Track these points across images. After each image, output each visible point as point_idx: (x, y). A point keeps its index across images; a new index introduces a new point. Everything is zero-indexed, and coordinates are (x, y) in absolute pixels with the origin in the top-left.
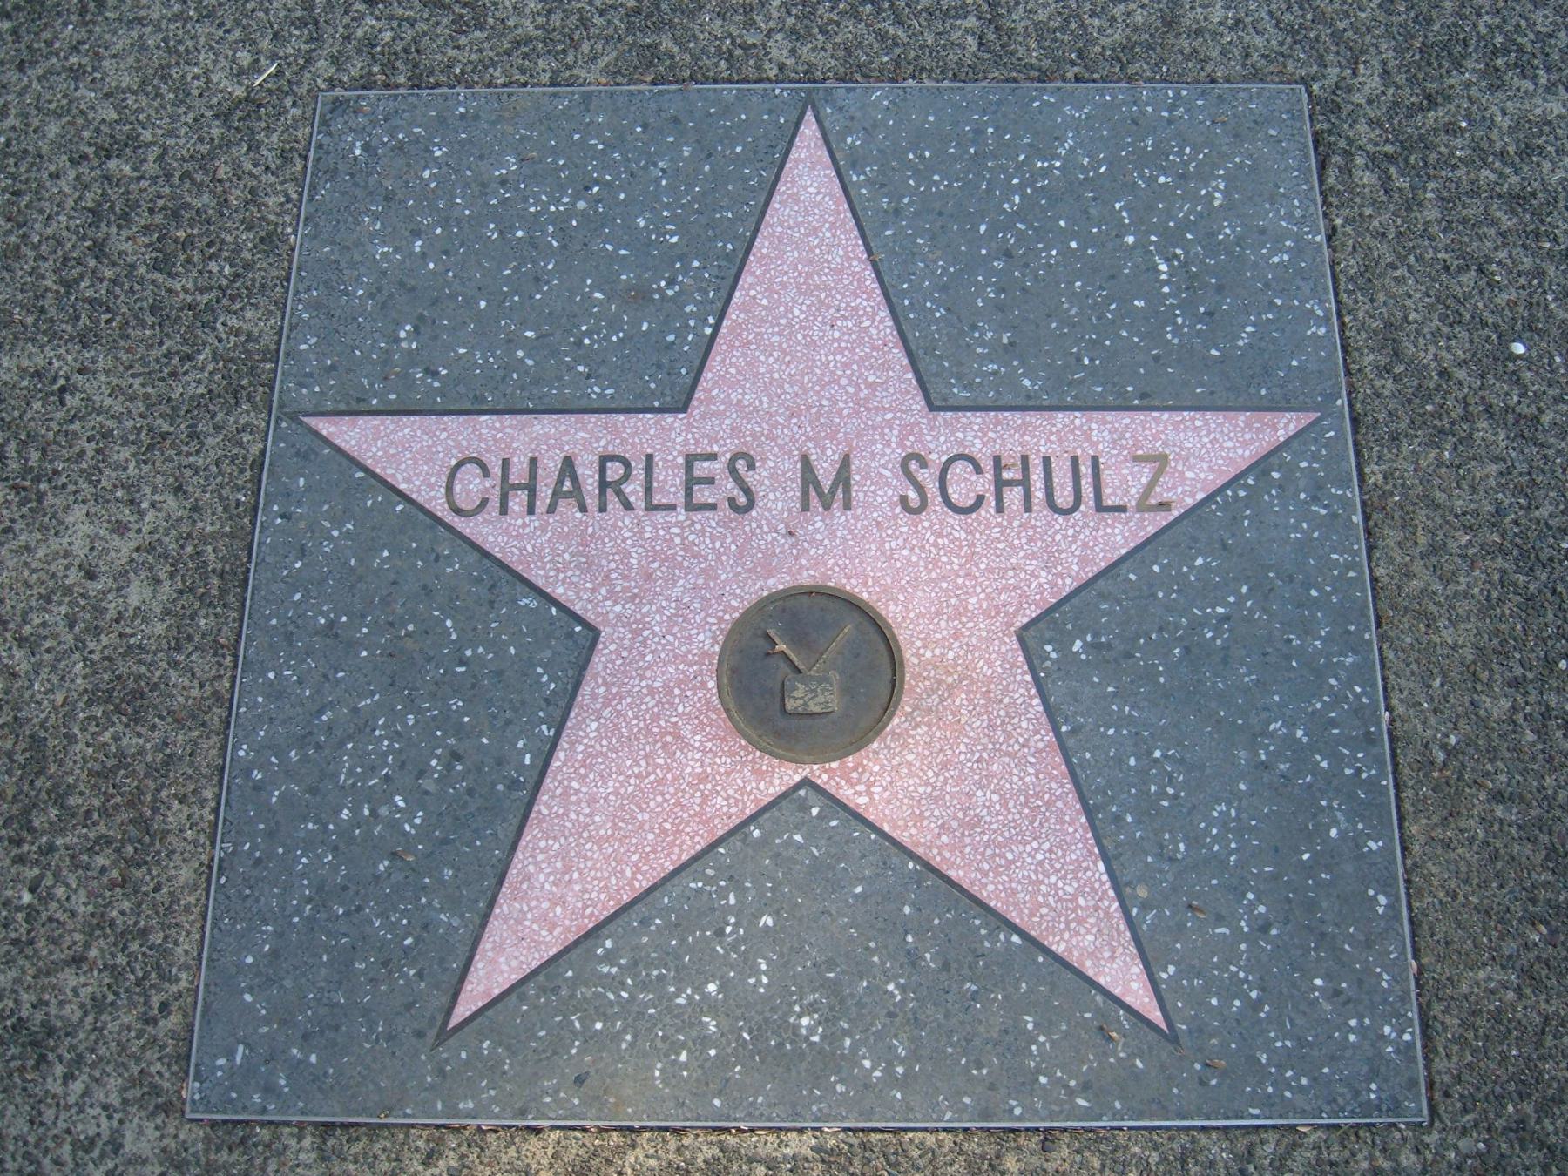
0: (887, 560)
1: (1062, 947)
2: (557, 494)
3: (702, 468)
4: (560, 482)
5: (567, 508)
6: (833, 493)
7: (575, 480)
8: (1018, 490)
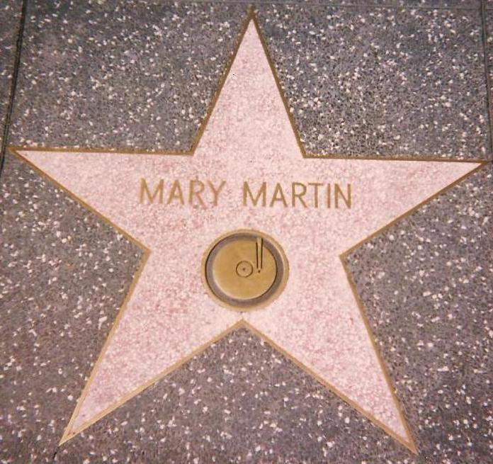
4: (275, 195)
6: (156, 192)
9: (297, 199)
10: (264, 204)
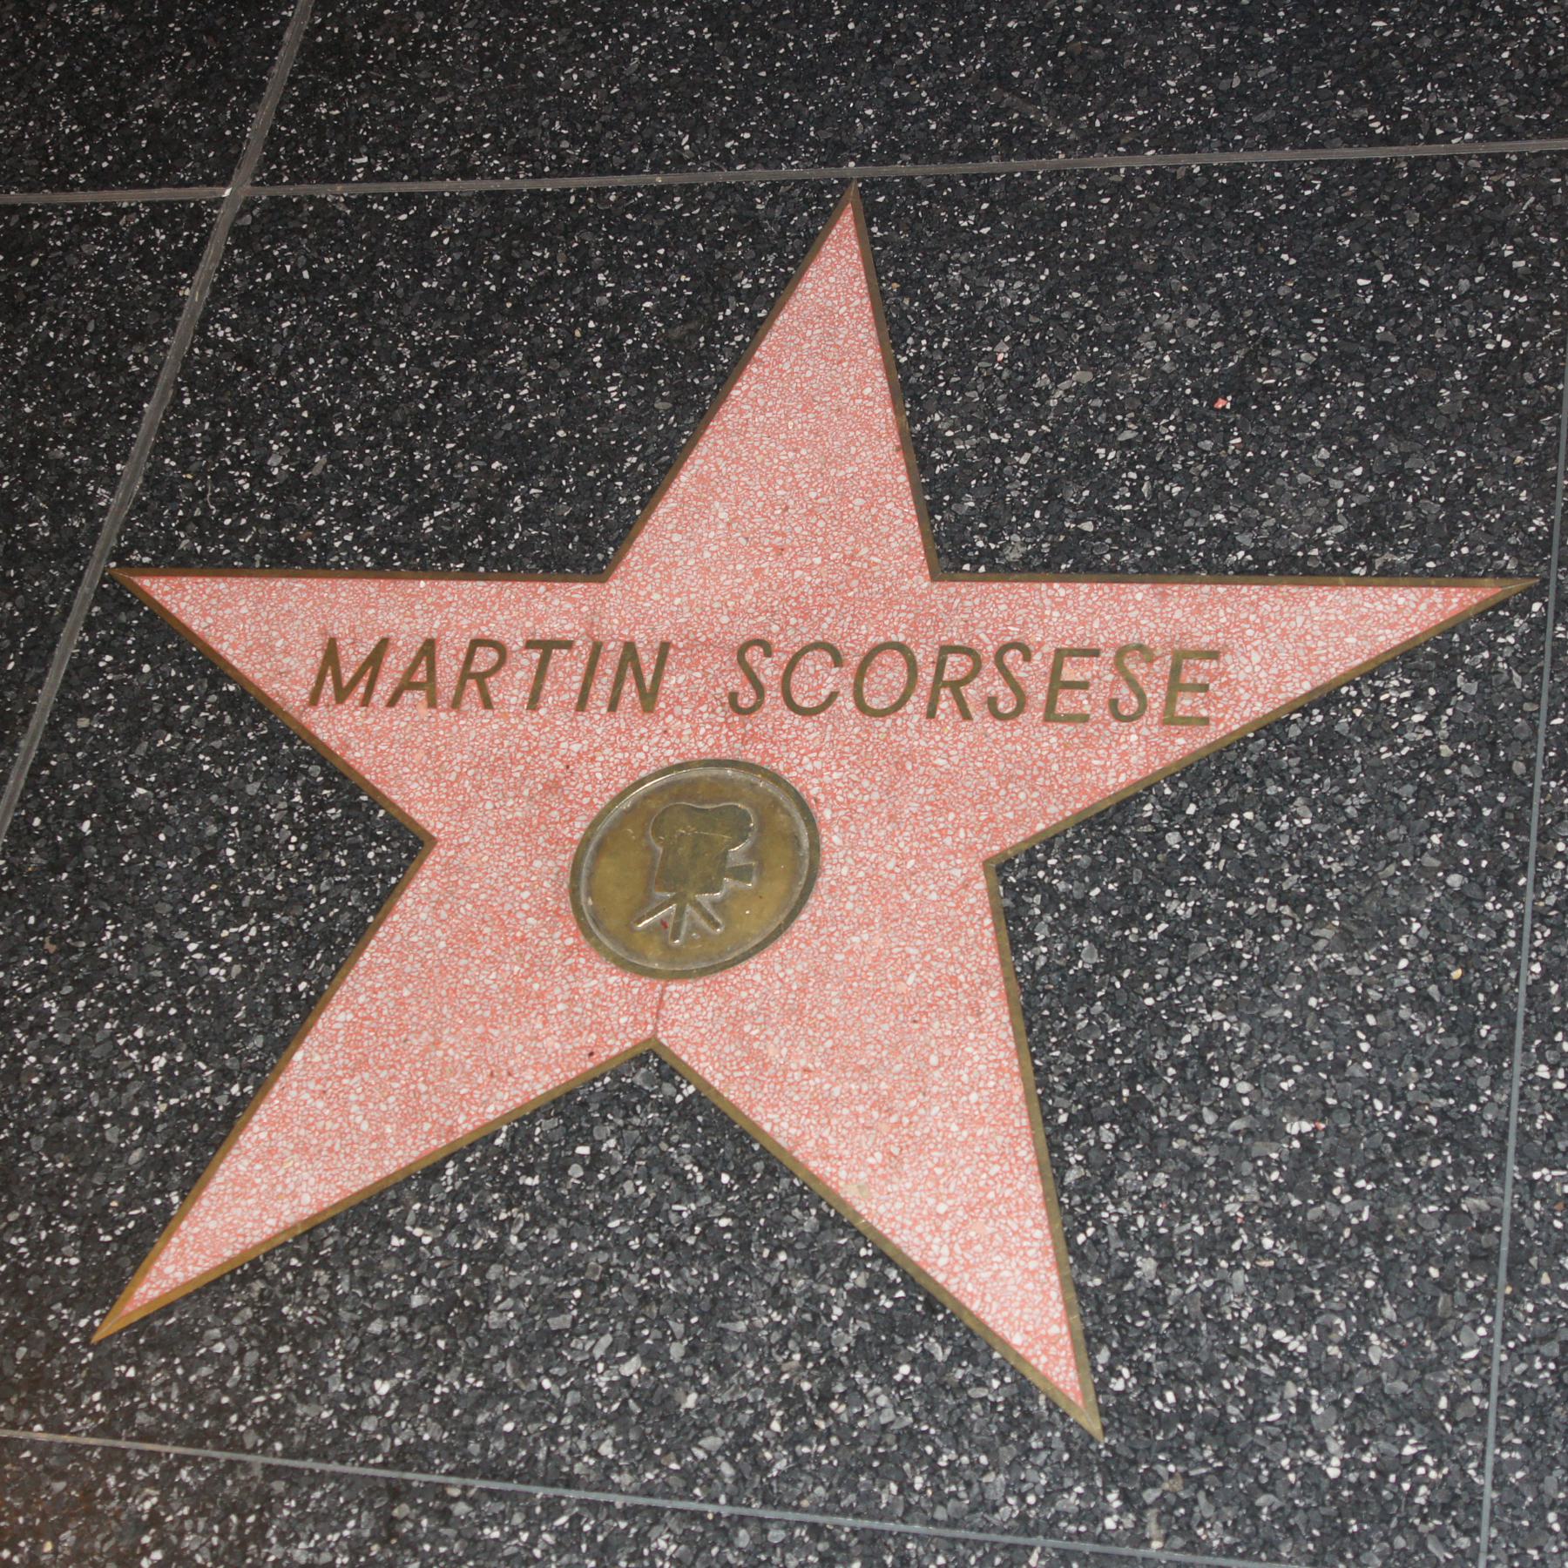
2: (406, 684)
3: (1069, 673)
6: (354, 682)
9: (945, 693)
10: (366, 701)
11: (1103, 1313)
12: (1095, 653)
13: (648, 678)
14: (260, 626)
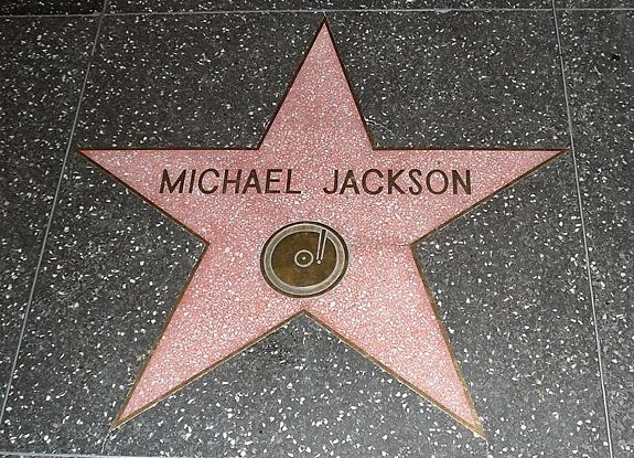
0: (343, 214)
1: (178, 379)
2: (248, 185)
4: (249, 180)
5: (349, 191)
6: (175, 185)
7: (256, 180)
8: (234, 185)
11: (151, 414)
12: (281, 171)
13: (465, 181)
14: (138, 168)
